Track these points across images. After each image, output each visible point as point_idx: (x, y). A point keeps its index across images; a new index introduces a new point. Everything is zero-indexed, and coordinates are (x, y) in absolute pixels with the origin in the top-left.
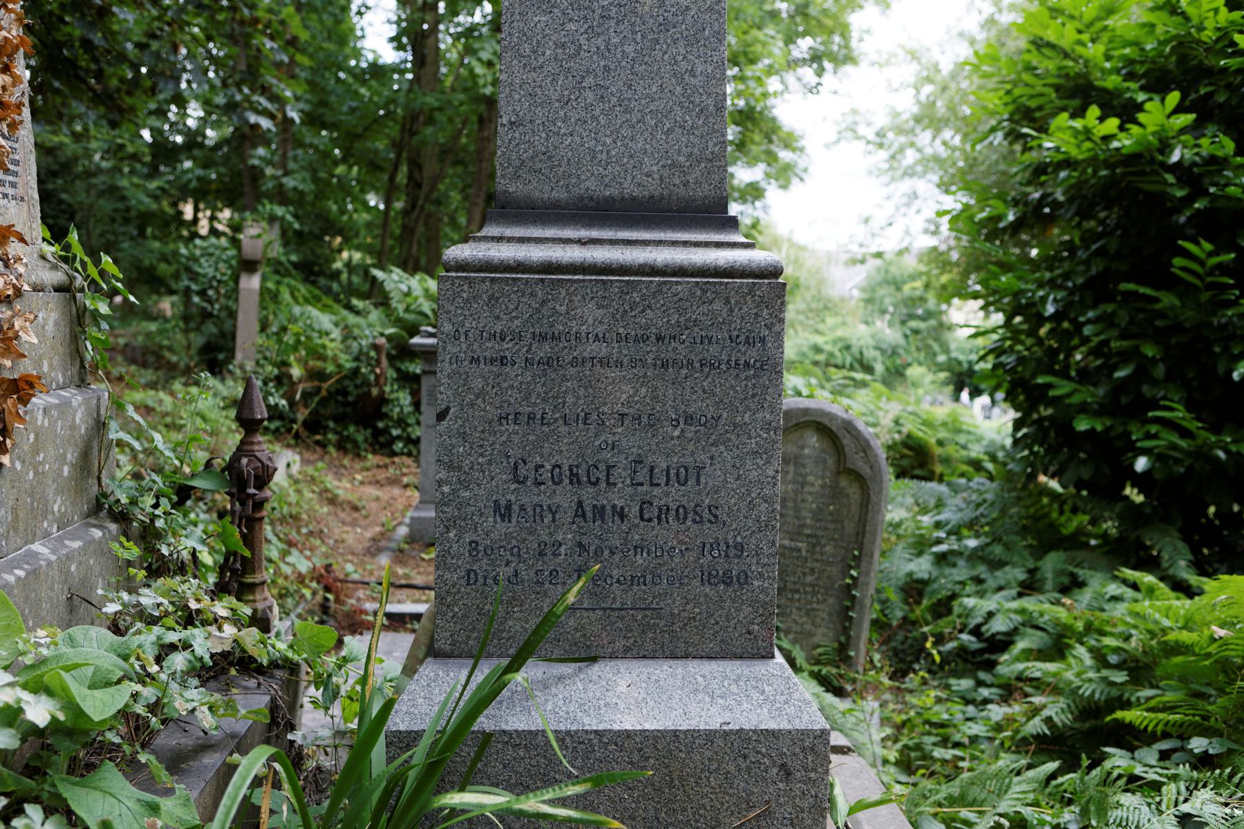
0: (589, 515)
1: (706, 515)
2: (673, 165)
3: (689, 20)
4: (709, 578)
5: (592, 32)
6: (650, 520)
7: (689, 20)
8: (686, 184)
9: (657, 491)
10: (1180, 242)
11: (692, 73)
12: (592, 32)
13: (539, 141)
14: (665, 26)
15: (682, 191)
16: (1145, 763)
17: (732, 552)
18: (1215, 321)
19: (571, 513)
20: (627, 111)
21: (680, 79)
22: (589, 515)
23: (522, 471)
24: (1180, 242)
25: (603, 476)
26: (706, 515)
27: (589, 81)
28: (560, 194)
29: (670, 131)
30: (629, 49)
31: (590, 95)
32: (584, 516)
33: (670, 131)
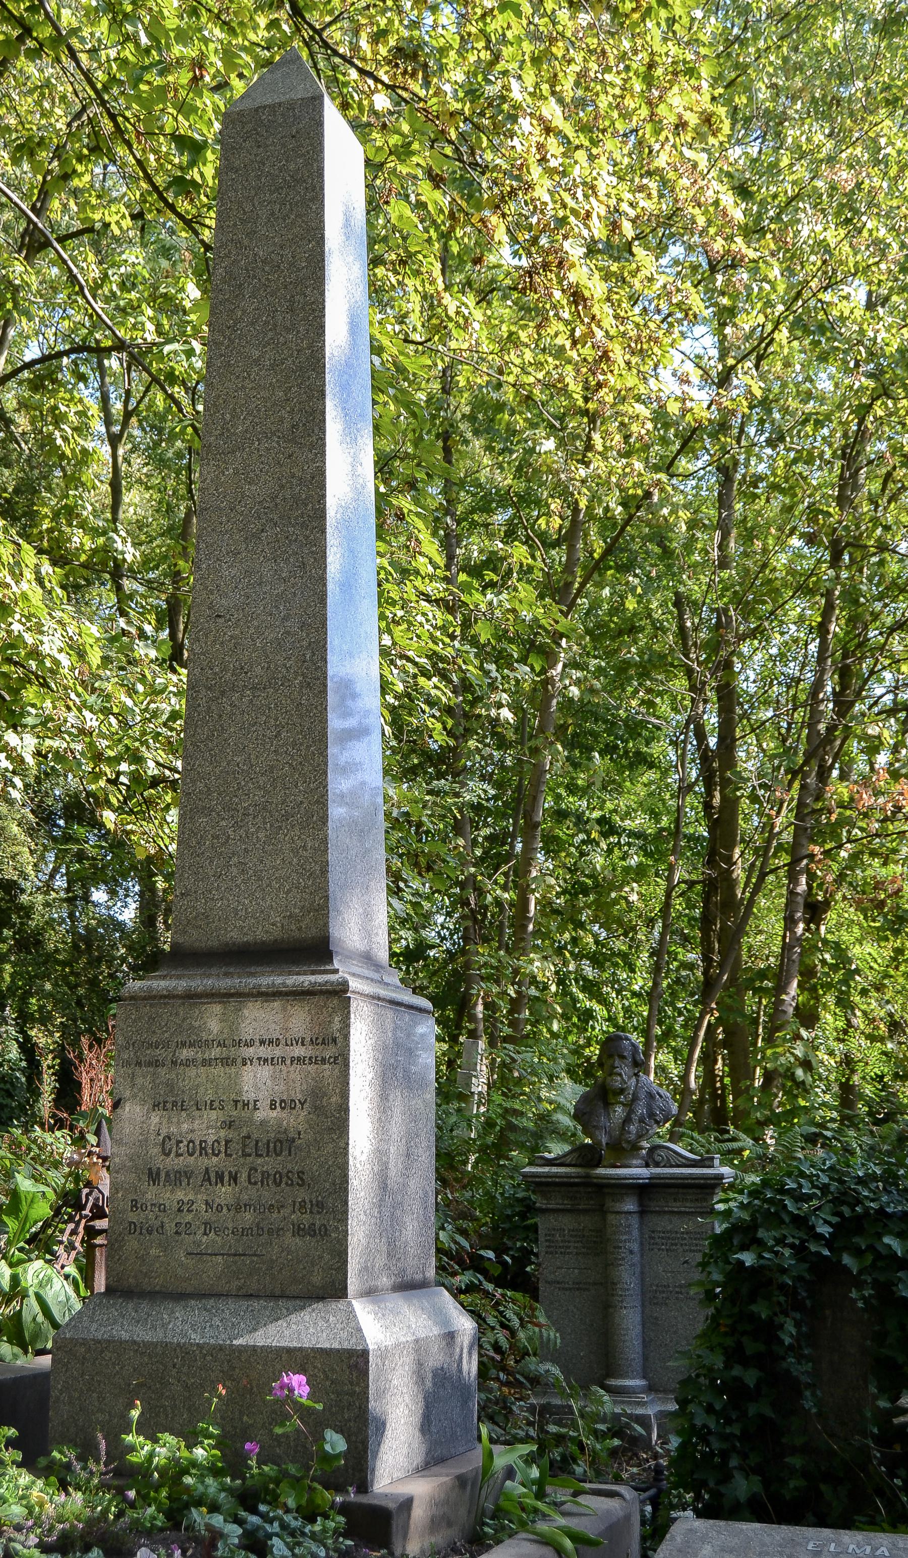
0: (213, 1180)
1: (296, 1180)
2: (290, 916)
3: (302, 811)
4: (299, 1231)
5: (237, 826)
6: (256, 1183)
7: (302, 811)
8: (300, 929)
9: (260, 1161)
10: (896, 1421)
11: (304, 848)
12: (237, 826)
13: (200, 906)
14: (286, 817)
15: (296, 934)
16: (790, 603)
17: (315, 1209)
18: (814, 1410)
19: (200, 1178)
20: (260, 879)
21: (295, 852)
22: (213, 1180)
23: (168, 1147)
24: (896, 1421)
25: (223, 1149)
26: (296, 1180)
27: (235, 860)
28: (213, 943)
29: (289, 891)
30: (261, 835)
31: (234, 870)
32: (209, 1180)
33: (289, 891)
